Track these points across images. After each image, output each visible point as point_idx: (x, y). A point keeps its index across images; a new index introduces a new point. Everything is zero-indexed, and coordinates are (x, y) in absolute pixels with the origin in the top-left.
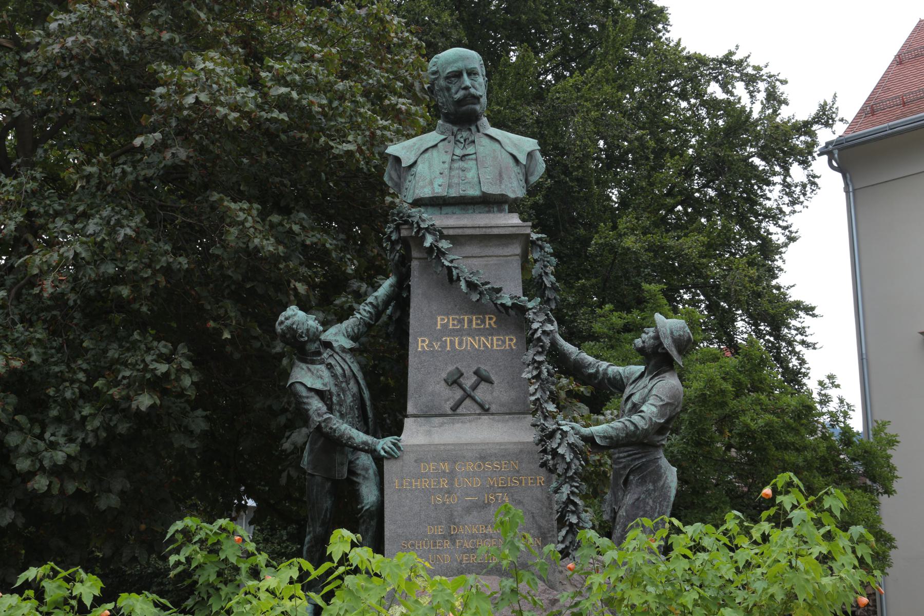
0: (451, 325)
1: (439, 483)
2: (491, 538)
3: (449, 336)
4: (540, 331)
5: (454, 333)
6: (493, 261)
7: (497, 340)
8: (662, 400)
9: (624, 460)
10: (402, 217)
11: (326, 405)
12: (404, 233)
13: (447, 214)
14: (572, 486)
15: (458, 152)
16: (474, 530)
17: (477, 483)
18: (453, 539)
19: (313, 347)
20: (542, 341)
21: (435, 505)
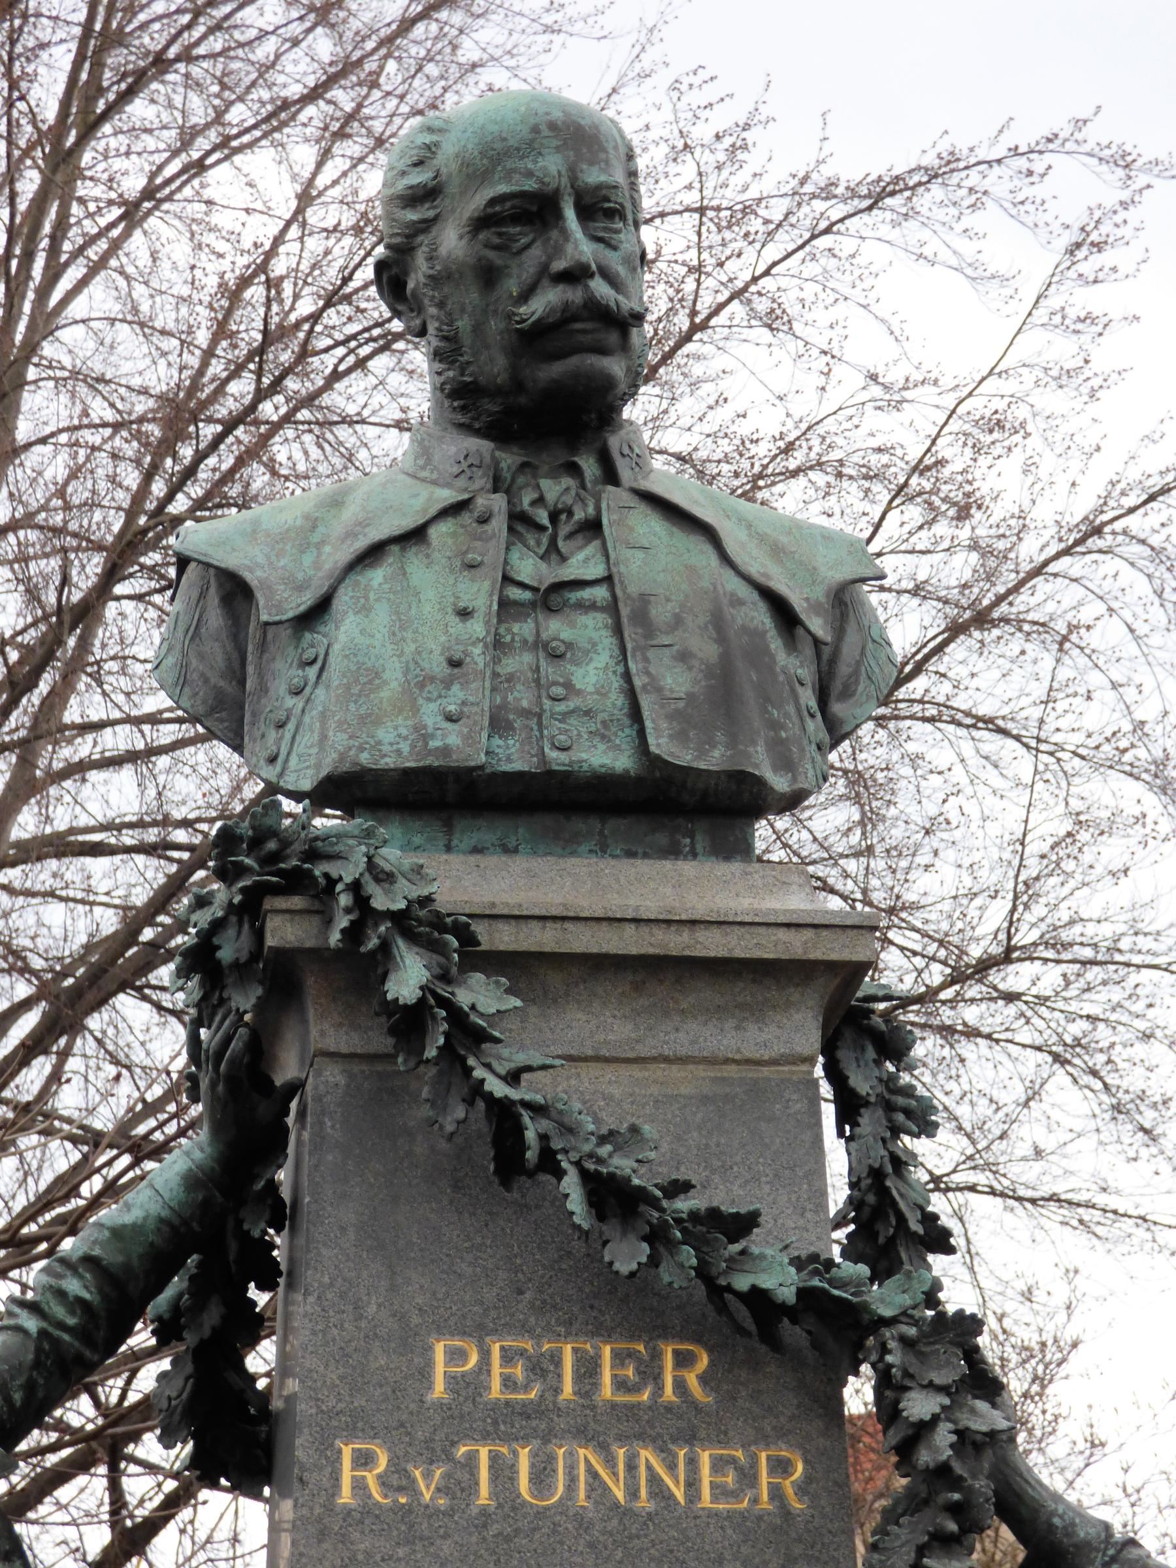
0: (496, 1384)
3: (485, 1437)
4: (944, 1437)
7: (718, 1465)
13: (477, 850)
20: (956, 1483)
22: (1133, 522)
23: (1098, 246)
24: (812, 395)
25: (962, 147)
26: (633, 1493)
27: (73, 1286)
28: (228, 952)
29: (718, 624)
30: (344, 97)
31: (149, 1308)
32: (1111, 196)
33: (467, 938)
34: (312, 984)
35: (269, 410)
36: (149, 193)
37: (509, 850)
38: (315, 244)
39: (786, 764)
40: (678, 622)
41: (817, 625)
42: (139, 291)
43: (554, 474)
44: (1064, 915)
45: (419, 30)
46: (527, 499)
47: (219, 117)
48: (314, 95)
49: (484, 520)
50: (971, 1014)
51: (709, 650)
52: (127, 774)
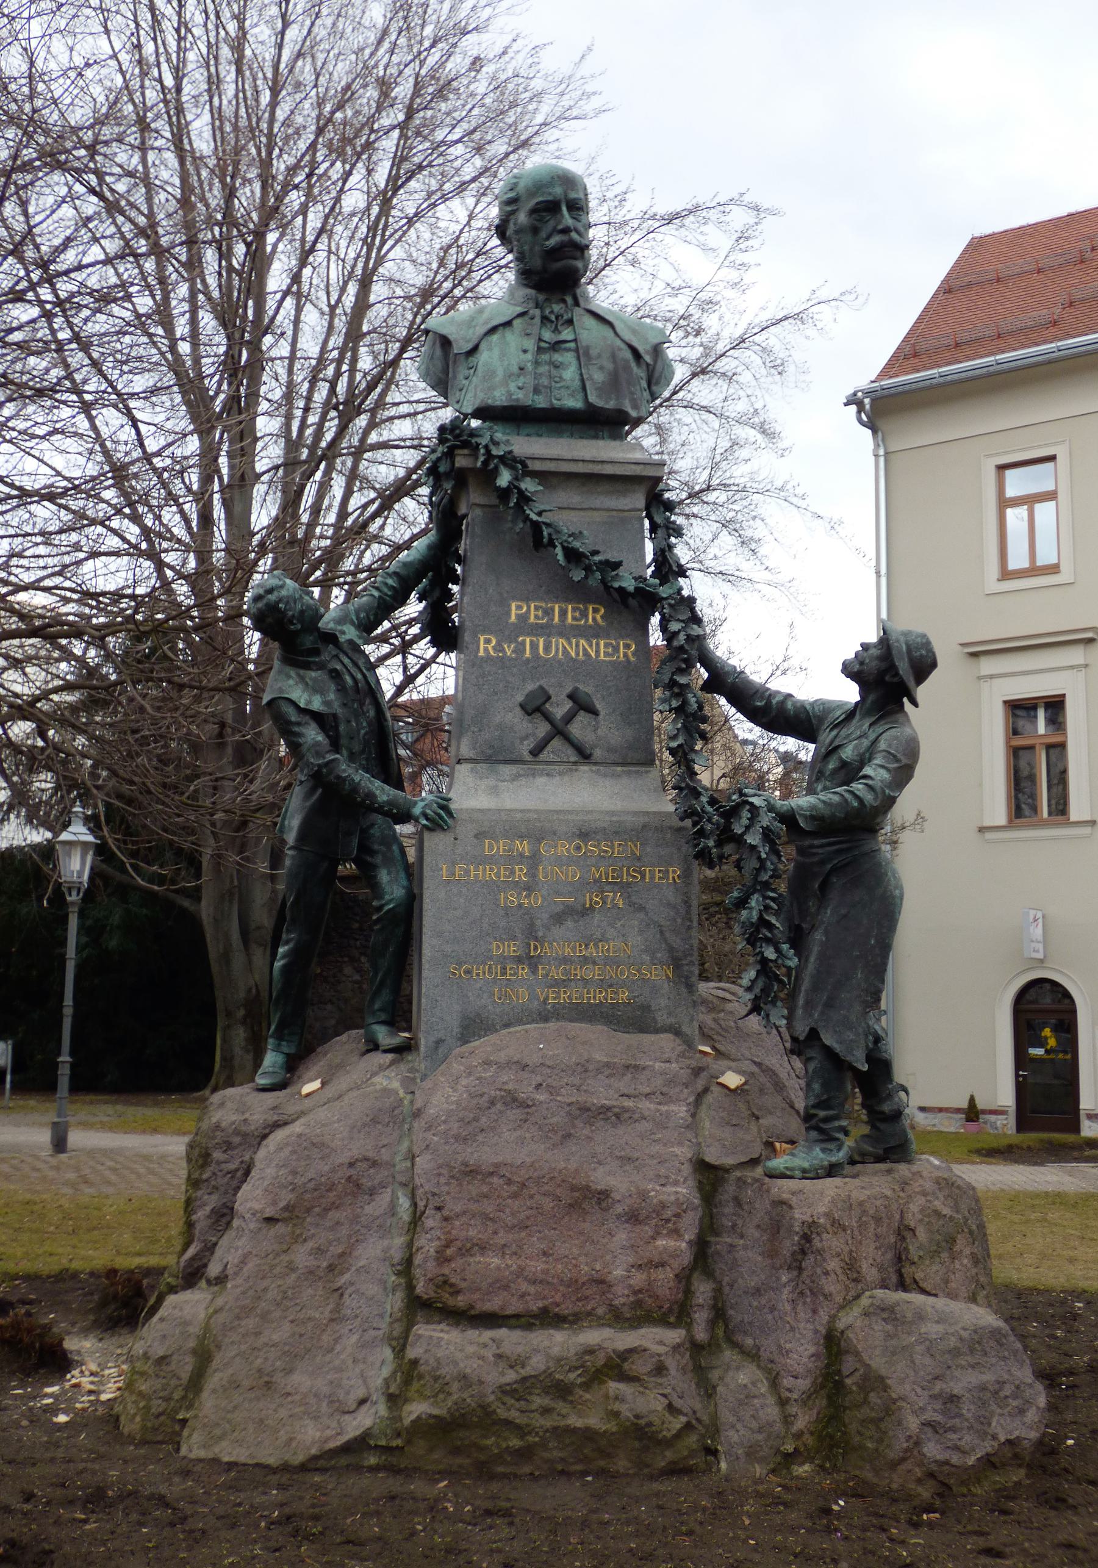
1: (513, 872)
2: (594, 963)
3: (528, 635)
4: (682, 637)
5: (536, 630)
6: (598, 516)
7: (606, 646)
8: (897, 760)
9: (820, 851)
10: (459, 435)
11: (328, 736)
12: (461, 461)
14: (765, 897)
15: (547, 335)
16: (567, 951)
17: (574, 874)
18: (533, 963)
19: (308, 641)
20: (686, 652)
21: (506, 908)
22: (757, 338)
23: (747, 238)
24: (646, 289)
25: (701, 203)
26: (577, 654)
27: (390, 582)
28: (442, 469)
29: (613, 357)
30: (485, 181)
32: (752, 221)
33: (525, 465)
34: (471, 481)
35: (458, 292)
36: (416, 214)
37: (540, 436)
38: (473, 233)
39: (636, 407)
40: (599, 356)
41: (648, 359)
42: (413, 249)
43: (557, 303)
44: (728, 474)
45: (511, 157)
46: (547, 312)
47: (440, 188)
48: (474, 180)
49: (532, 318)
50: (695, 510)
51: (610, 366)
52: (408, 421)
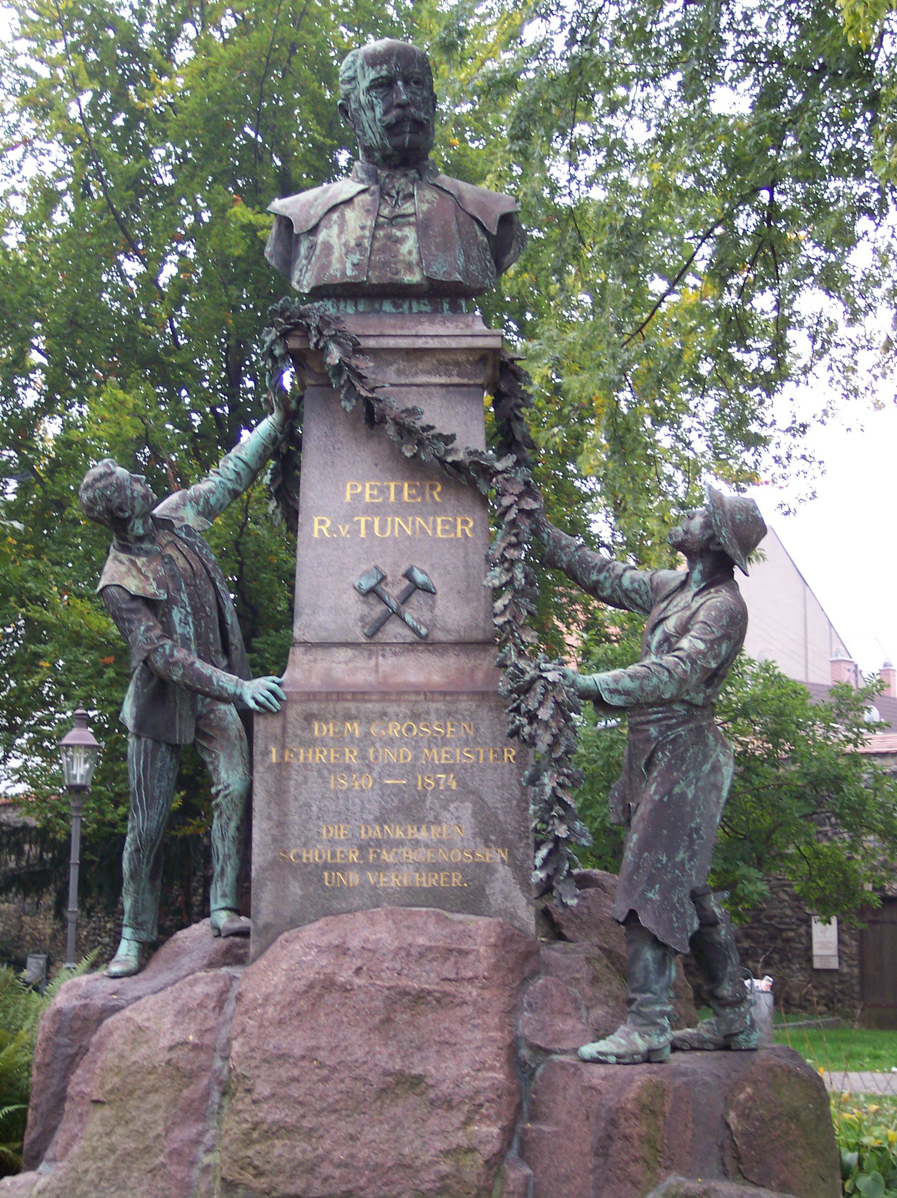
7: (444, 523)
10: (289, 318)
26: (414, 532)
28: (278, 352)
31: (631, 667)
